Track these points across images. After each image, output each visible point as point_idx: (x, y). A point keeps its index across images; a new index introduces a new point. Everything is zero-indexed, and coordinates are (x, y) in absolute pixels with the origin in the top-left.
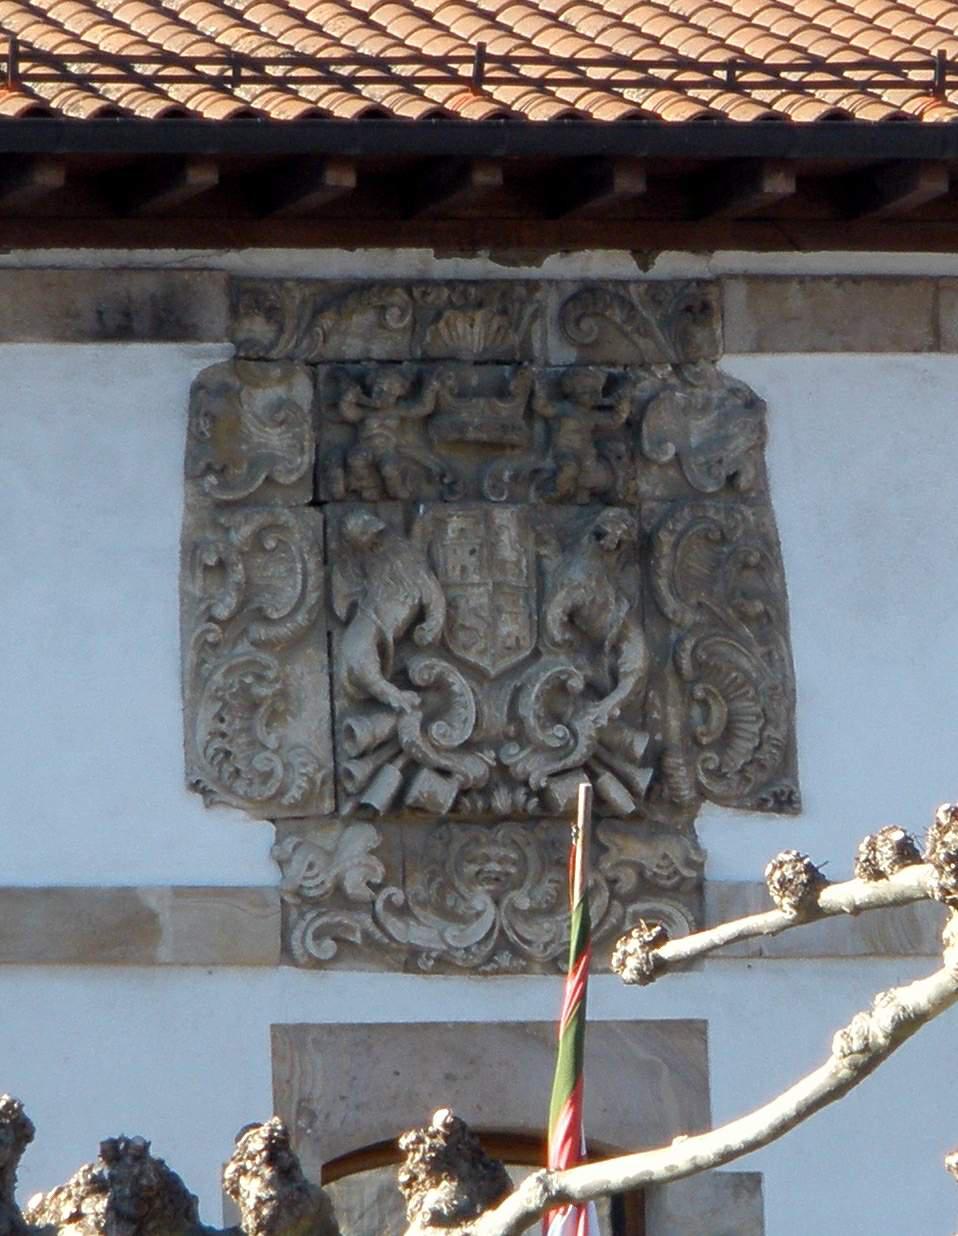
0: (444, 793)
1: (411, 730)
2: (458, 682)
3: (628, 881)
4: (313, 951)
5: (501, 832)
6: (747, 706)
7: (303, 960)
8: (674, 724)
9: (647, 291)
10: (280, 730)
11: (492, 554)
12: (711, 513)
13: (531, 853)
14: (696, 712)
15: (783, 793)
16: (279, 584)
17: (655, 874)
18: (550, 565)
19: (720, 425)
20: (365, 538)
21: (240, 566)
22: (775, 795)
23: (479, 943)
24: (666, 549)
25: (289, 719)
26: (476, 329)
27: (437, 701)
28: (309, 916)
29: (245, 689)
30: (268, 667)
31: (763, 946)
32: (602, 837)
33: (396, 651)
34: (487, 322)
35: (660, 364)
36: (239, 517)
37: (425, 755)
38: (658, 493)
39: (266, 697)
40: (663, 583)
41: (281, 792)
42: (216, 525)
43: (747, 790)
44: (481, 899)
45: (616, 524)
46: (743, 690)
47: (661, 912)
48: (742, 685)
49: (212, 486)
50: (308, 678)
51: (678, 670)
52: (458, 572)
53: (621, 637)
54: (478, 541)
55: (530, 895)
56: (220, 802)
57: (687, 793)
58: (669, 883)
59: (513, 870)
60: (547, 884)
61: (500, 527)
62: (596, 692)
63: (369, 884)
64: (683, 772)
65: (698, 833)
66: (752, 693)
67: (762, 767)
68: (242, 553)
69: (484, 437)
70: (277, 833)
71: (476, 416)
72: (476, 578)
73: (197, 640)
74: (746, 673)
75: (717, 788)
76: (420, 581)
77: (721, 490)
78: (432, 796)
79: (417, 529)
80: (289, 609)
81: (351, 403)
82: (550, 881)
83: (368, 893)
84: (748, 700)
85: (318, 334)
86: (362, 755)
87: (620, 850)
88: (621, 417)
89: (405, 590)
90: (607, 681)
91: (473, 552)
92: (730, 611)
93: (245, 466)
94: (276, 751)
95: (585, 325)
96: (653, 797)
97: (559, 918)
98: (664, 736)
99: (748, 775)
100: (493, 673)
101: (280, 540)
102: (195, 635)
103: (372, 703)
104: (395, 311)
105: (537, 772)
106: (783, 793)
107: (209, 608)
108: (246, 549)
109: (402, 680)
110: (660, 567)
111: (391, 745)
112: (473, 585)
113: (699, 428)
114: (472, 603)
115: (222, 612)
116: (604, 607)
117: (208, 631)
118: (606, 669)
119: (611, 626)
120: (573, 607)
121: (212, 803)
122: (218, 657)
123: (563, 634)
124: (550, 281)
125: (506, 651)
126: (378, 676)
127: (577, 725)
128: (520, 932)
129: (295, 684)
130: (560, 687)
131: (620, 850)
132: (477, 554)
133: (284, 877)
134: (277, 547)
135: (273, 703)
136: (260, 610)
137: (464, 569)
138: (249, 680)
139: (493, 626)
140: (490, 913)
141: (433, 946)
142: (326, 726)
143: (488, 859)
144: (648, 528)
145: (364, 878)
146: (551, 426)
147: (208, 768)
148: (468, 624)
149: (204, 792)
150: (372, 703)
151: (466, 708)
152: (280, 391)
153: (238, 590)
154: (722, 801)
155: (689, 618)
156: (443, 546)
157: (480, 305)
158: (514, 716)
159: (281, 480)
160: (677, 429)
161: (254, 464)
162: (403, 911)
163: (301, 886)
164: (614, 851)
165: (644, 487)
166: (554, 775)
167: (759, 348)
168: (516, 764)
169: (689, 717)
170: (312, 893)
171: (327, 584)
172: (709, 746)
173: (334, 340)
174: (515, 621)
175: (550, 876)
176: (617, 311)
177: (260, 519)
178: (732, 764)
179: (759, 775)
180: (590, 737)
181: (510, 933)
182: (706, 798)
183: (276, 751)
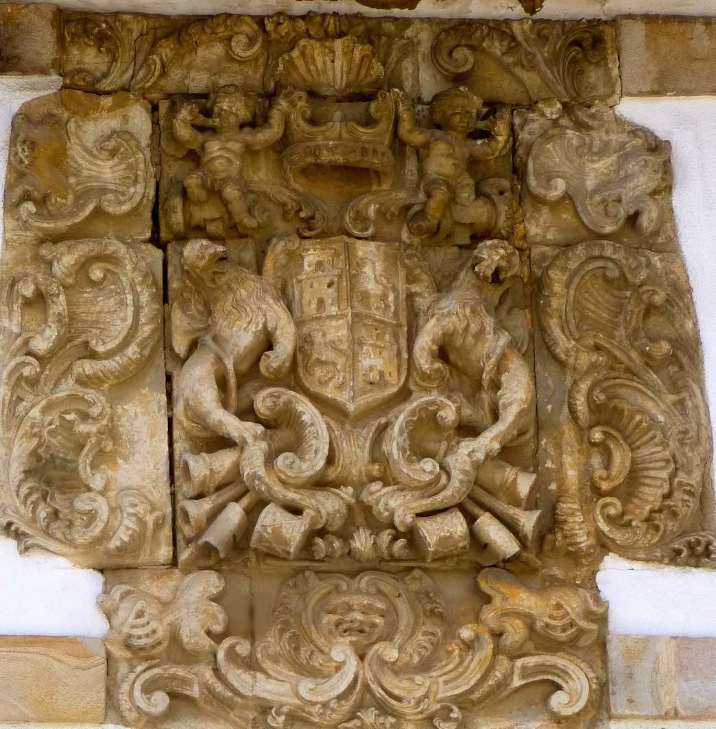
0: (293, 530)
1: (254, 459)
2: (308, 411)
3: (515, 633)
4: (142, 704)
5: (364, 581)
6: (652, 452)
7: (132, 716)
8: (572, 474)
9: (532, 29)
10: (109, 472)
11: (352, 288)
12: (609, 252)
13: (403, 606)
14: (596, 461)
15: (698, 542)
16: (108, 318)
17: (547, 625)
18: (422, 303)
19: (620, 165)
20: (202, 263)
21: (62, 298)
22: (691, 547)
23: (340, 698)
24: (558, 288)
25: (120, 461)
26: (338, 63)
27: (282, 430)
28: (139, 669)
29: (68, 426)
30: (93, 404)
31: (678, 704)
32: (484, 586)
33: (239, 386)
34: (348, 53)
35: (547, 100)
36: (61, 247)
37: (269, 488)
38: (550, 236)
39: (88, 435)
40: (554, 324)
41: (105, 537)
42: (37, 259)
43: (655, 540)
44: (342, 651)
45: (233, 107)
46: (650, 434)
47: (555, 667)
48: (649, 428)
49: (30, 214)
50: (141, 418)
51: (573, 411)
52: (314, 306)
53: (500, 368)
54: (336, 272)
55: (401, 649)
56: (39, 546)
57: (584, 540)
58: (563, 636)
59: (378, 620)
60: (420, 637)
61: (362, 259)
62: (468, 430)
63: (209, 633)
64: (579, 518)
65: (600, 587)
66: (659, 435)
67: (675, 514)
68: (66, 288)
69: (340, 159)
70: (105, 583)
71: (334, 138)
72: (334, 310)
73: (10, 375)
74: (653, 418)
75: (618, 536)
76: (264, 306)
77: (622, 228)
78: (277, 532)
79: (269, 264)
80: (117, 342)
81: (184, 121)
82: (425, 634)
83: (207, 642)
84: (656, 445)
85: (155, 63)
86: (200, 496)
87: (505, 599)
88: (498, 142)
89: (247, 315)
90: (486, 414)
91: (330, 285)
92: (634, 355)
93: (71, 197)
94: (103, 493)
95: (459, 54)
96: (547, 547)
97: (434, 674)
98: (559, 487)
99: (657, 522)
100: (351, 407)
101: (108, 270)
102: (9, 368)
103: (218, 442)
104: (243, 39)
105: (402, 509)
106: (698, 542)
107: (26, 342)
108: (70, 281)
109: (247, 413)
110: (550, 305)
111: (234, 484)
112: (331, 317)
113: (597, 170)
114: (329, 337)
115: (41, 345)
116: (480, 334)
117: (24, 364)
118: (486, 406)
119: (489, 358)
120: (444, 335)
121: (27, 549)
122: (37, 395)
123: (432, 363)
124: (422, 20)
125: (369, 387)
126: (214, 404)
127: (451, 461)
128: (388, 687)
129: (127, 424)
130: (428, 420)
131: (505, 599)
132: (335, 285)
133: (111, 627)
134: (105, 277)
135: (99, 443)
136: (86, 344)
137: (321, 303)
138: (71, 417)
139: (353, 358)
140: (352, 664)
141: (284, 699)
142: (164, 468)
143: (350, 609)
144: (538, 272)
145: (203, 627)
146: (421, 153)
147: (22, 510)
148: (323, 358)
149: (18, 536)
150: (218, 442)
151: (317, 438)
152: (112, 123)
153: (59, 321)
154: (627, 552)
155: (585, 359)
156: (299, 281)
157: (341, 35)
158: (377, 455)
159: (110, 210)
160: (567, 166)
161: (82, 197)
162: (251, 664)
163: (130, 636)
164: (497, 601)
165: (534, 230)
166: (420, 515)
167: (658, 91)
168: (378, 502)
169: (588, 465)
170: (142, 642)
171: (165, 323)
172: (611, 493)
173: (175, 74)
174: (380, 350)
175: (424, 628)
176: (497, 44)
177: (84, 248)
178: (638, 511)
179: (670, 524)
180: (465, 472)
181: (375, 687)
182: (610, 551)
183: (103, 493)
